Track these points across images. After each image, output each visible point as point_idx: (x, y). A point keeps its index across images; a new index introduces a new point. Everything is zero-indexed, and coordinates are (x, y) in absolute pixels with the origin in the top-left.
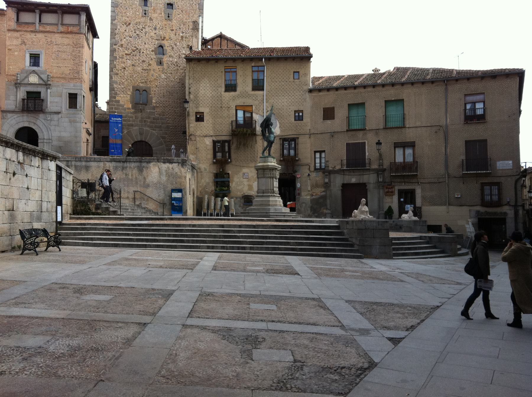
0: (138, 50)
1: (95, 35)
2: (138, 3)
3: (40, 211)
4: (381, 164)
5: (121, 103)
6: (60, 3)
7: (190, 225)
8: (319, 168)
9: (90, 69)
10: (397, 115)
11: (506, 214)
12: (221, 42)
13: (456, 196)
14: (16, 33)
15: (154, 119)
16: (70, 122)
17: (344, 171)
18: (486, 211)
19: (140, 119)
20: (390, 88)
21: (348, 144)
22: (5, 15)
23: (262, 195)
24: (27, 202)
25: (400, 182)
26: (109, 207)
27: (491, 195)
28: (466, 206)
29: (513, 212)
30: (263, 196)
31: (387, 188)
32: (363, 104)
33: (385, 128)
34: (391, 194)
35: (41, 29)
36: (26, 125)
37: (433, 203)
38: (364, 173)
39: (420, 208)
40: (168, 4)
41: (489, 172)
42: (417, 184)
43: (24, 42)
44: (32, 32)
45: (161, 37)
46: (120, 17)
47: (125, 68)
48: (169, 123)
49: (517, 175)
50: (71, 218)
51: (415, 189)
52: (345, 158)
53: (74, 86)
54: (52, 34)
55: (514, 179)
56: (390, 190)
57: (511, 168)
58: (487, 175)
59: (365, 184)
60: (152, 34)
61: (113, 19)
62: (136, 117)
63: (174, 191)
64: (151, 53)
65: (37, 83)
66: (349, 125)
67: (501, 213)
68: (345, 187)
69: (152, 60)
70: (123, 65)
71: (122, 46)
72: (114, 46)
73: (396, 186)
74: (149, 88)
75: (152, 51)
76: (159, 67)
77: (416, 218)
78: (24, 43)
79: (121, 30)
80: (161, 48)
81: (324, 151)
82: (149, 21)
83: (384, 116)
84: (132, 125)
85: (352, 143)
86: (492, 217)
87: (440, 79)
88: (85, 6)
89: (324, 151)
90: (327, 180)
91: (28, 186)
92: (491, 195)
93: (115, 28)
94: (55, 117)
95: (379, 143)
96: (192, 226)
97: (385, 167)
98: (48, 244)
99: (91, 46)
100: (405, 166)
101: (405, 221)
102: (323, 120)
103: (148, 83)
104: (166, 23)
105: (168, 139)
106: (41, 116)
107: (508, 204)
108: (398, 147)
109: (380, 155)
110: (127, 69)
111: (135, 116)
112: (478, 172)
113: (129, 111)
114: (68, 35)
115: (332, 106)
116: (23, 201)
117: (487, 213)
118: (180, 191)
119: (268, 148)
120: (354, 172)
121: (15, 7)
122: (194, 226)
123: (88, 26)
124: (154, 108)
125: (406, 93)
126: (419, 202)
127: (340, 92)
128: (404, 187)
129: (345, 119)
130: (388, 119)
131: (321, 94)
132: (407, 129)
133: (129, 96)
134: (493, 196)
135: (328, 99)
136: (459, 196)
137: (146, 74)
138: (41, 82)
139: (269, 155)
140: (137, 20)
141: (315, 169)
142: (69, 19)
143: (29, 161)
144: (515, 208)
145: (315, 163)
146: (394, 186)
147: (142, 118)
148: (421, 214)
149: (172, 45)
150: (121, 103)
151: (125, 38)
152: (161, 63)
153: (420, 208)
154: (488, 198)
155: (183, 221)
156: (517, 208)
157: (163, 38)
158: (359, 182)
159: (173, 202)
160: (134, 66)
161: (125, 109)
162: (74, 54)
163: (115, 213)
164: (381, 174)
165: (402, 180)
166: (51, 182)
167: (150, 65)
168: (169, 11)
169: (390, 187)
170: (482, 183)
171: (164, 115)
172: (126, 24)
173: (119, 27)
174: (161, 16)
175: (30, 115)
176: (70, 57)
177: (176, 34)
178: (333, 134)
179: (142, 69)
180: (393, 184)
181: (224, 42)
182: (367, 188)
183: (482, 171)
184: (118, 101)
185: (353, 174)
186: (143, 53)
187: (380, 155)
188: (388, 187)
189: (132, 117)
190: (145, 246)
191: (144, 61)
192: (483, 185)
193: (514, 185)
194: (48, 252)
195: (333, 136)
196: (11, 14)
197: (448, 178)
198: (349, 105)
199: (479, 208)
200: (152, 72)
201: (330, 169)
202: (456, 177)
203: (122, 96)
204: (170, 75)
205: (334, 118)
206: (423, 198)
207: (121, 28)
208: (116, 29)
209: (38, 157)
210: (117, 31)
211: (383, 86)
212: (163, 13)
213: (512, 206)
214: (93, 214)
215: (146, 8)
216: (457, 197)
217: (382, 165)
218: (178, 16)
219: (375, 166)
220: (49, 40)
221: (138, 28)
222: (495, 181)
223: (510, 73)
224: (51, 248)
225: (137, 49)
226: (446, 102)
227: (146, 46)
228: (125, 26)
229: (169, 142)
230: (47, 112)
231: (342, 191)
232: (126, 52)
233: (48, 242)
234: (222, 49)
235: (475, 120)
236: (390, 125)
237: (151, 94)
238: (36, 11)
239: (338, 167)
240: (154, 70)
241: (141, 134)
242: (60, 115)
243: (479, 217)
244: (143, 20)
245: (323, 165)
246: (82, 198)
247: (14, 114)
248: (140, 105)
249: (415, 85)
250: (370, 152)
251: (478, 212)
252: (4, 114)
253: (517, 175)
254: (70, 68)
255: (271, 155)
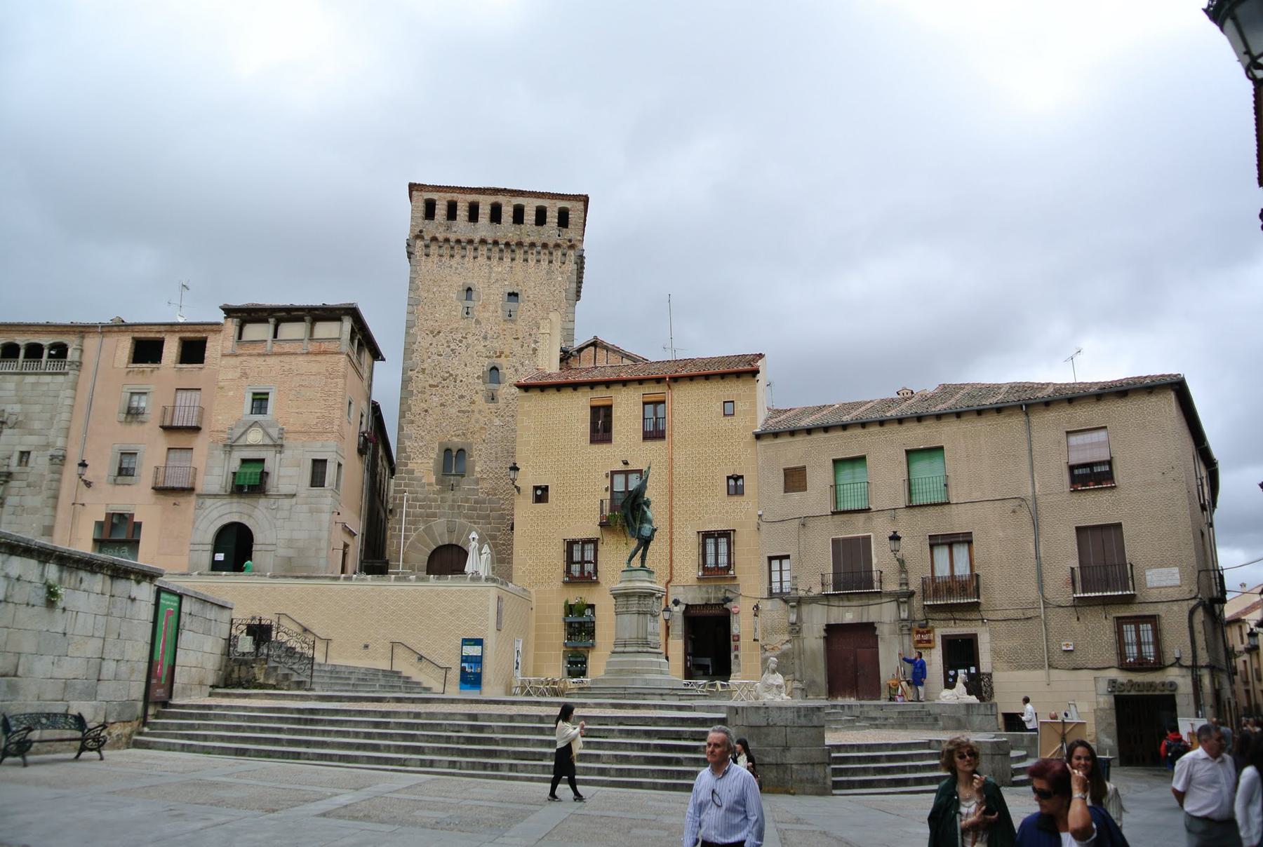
0: (451, 378)
1: (376, 355)
2: (454, 296)
3: (96, 677)
4: (904, 581)
5: (417, 474)
6: (310, 304)
7: (408, 714)
8: (778, 591)
9: (362, 416)
10: (938, 479)
11: (1173, 685)
12: (595, 355)
13: (1064, 648)
14: (235, 358)
15: (476, 502)
16: (311, 511)
17: (829, 597)
18: (1130, 681)
19: (450, 502)
20: (914, 425)
21: (835, 542)
22: (221, 331)
23: (622, 649)
24: (59, 660)
25: (944, 620)
26: (292, 675)
27: (1139, 644)
28: (1086, 668)
29: (1189, 680)
30: (624, 652)
31: (918, 633)
32: (862, 459)
33: (910, 507)
34: (928, 645)
35: (276, 349)
36: (236, 519)
37: (1016, 663)
38: (871, 602)
39: (990, 675)
40: (510, 294)
41: (1128, 592)
42: (980, 622)
43: (245, 373)
44: (259, 355)
45: (495, 353)
46: (422, 321)
47: (426, 411)
48: (504, 510)
49: (1191, 599)
50: (210, 695)
51: (975, 635)
52: (831, 570)
53: (323, 446)
54: (293, 357)
55: (1186, 607)
56: (925, 637)
57: (1178, 583)
58: (1129, 600)
59: (872, 624)
60: (480, 348)
61: (410, 326)
62: (443, 500)
63: (466, 642)
64: (477, 381)
65: (261, 443)
66: (836, 502)
67: (1163, 684)
68: (832, 631)
69: (477, 393)
70: (425, 406)
71: (424, 370)
72: (410, 373)
73: (937, 627)
74: (470, 445)
75: (478, 378)
76: (491, 405)
77: (973, 699)
78: (245, 375)
79: (422, 344)
80: (495, 371)
81: (787, 557)
82: (474, 325)
83: (906, 482)
84: (434, 515)
85: (845, 540)
86: (1145, 693)
87: (1014, 403)
88: (350, 306)
89: (787, 557)
90: (793, 618)
91: (65, 629)
92: (1139, 644)
93: (414, 341)
94: (286, 503)
95: (895, 538)
96: (412, 716)
97: (912, 588)
98: (83, 744)
99: (366, 375)
100: (954, 586)
101: (945, 705)
102: (785, 492)
103: (469, 435)
104: (505, 327)
105: (500, 539)
106: (263, 501)
107: (1177, 663)
108: (938, 545)
109: (901, 562)
110: (430, 412)
111: (441, 498)
112: (1105, 594)
113: (431, 488)
114: (319, 358)
115: (801, 465)
116: (48, 659)
117: (1132, 684)
118: (479, 642)
119: (641, 551)
120: (849, 600)
121: (237, 317)
122: (417, 715)
123: (359, 339)
124: (477, 481)
125: (943, 433)
126: (985, 662)
127: (815, 436)
128: (955, 630)
129: (828, 489)
130: (913, 488)
131: (778, 441)
132: (954, 506)
133: (432, 461)
134: (1143, 647)
135: (793, 452)
136: (1071, 648)
137: (465, 420)
138: (268, 441)
139: (643, 565)
140: (455, 325)
141: (771, 595)
142: (325, 329)
143: (75, 581)
144: (1192, 673)
145: (771, 582)
146: (933, 628)
147: (453, 501)
148: (992, 689)
149: (516, 365)
150: (417, 474)
151: (429, 358)
152: (493, 399)
153: (990, 675)
154: (1132, 651)
155: (347, 704)
156: (1199, 673)
157: (498, 354)
158: (859, 621)
159: (463, 665)
160: (444, 406)
161: (423, 486)
162: (326, 389)
163: (299, 685)
164: (905, 602)
165: (949, 615)
166: (136, 621)
167: (473, 402)
168: (512, 305)
169: (925, 630)
170: (1118, 618)
171: (496, 495)
172: (432, 332)
173: (419, 339)
174: (496, 317)
175: (242, 500)
176: (319, 395)
177: (522, 346)
178: (804, 522)
179: (459, 411)
180: (931, 623)
181: (602, 354)
182: (877, 633)
183: (1114, 591)
184: (412, 472)
185: (847, 603)
186: (461, 381)
187: (901, 562)
188: (921, 630)
189: (435, 500)
190: (297, 756)
191: (462, 397)
192: (1120, 621)
193: (1187, 620)
194: (81, 760)
195: (804, 525)
196: (231, 326)
197: (1045, 608)
198: (835, 462)
199: (1114, 674)
200: (477, 415)
201: (802, 593)
202: (1059, 606)
203: (419, 461)
204: (510, 419)
205: (806, 490)
206: (995, 652)
207: (423, 341)
208: (414, 343)
209: (102, 573)
210: (415, 347)
211: (900, 421)
212: (500, 310)
213: (1187, 667)
214: (262, 686)
215: (470, 304)
216: (1065, 651)
217: (907, 584)
218: (529, 313)
219: (892, 586)
220: (287, 367)
221: (454, 339)
222: (1147, 613)
223: (1154, 383)
224: (85, 755)
225: (451, 375)
226: (1031, 450)
227: (468, 369)
228: (431, 335)
229: (503, 545)
230: (271, 495)
231: (827, 639)
232: (431, 382)
233: (83, 740)
234: (596, 368)
235: (1091, 483)
236: (918, 500)
237: (472, 456)
238: (270, 320)
239: (816, 590)
240: (480, 411)
241: (451, 531)
242: (294, 500)
243: (1116, 693)
244: (462, 323)
245: (787, 586)
246: (244, 654)
247: (216, 500)
248: (452, 478)
249: (964, 418)
250: (881, 559)
251: (1113, 682)
252: (201, 501)
253: (1191, 599)
254: (319, 414)
255: (646, 565)
